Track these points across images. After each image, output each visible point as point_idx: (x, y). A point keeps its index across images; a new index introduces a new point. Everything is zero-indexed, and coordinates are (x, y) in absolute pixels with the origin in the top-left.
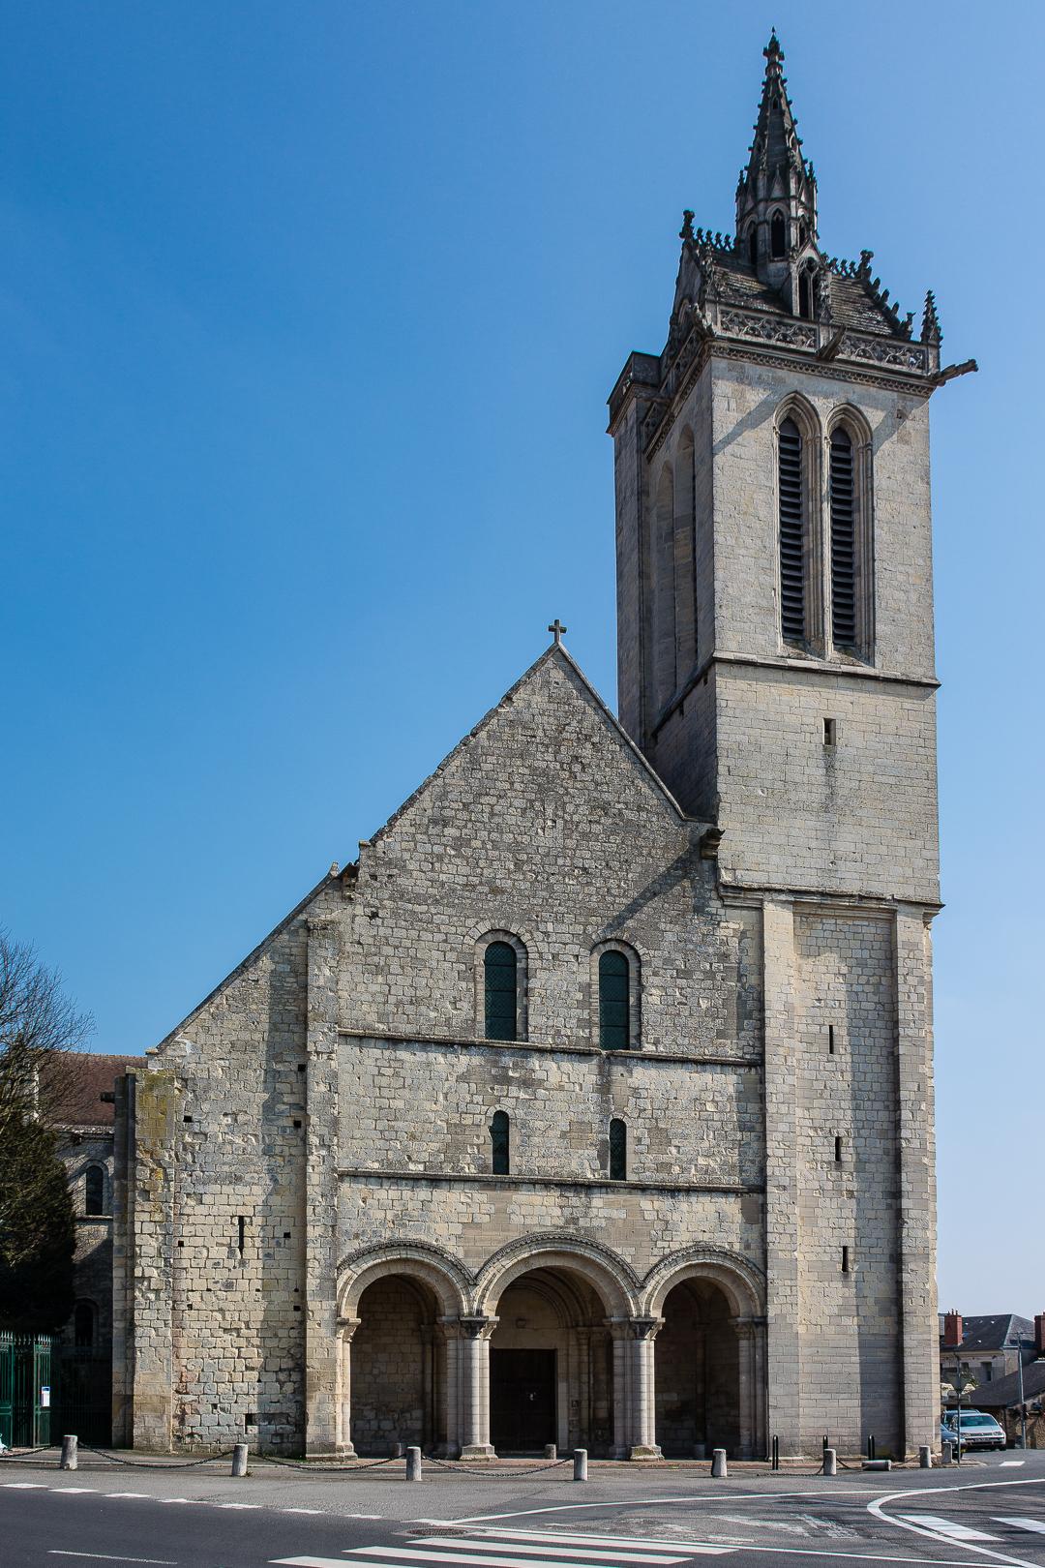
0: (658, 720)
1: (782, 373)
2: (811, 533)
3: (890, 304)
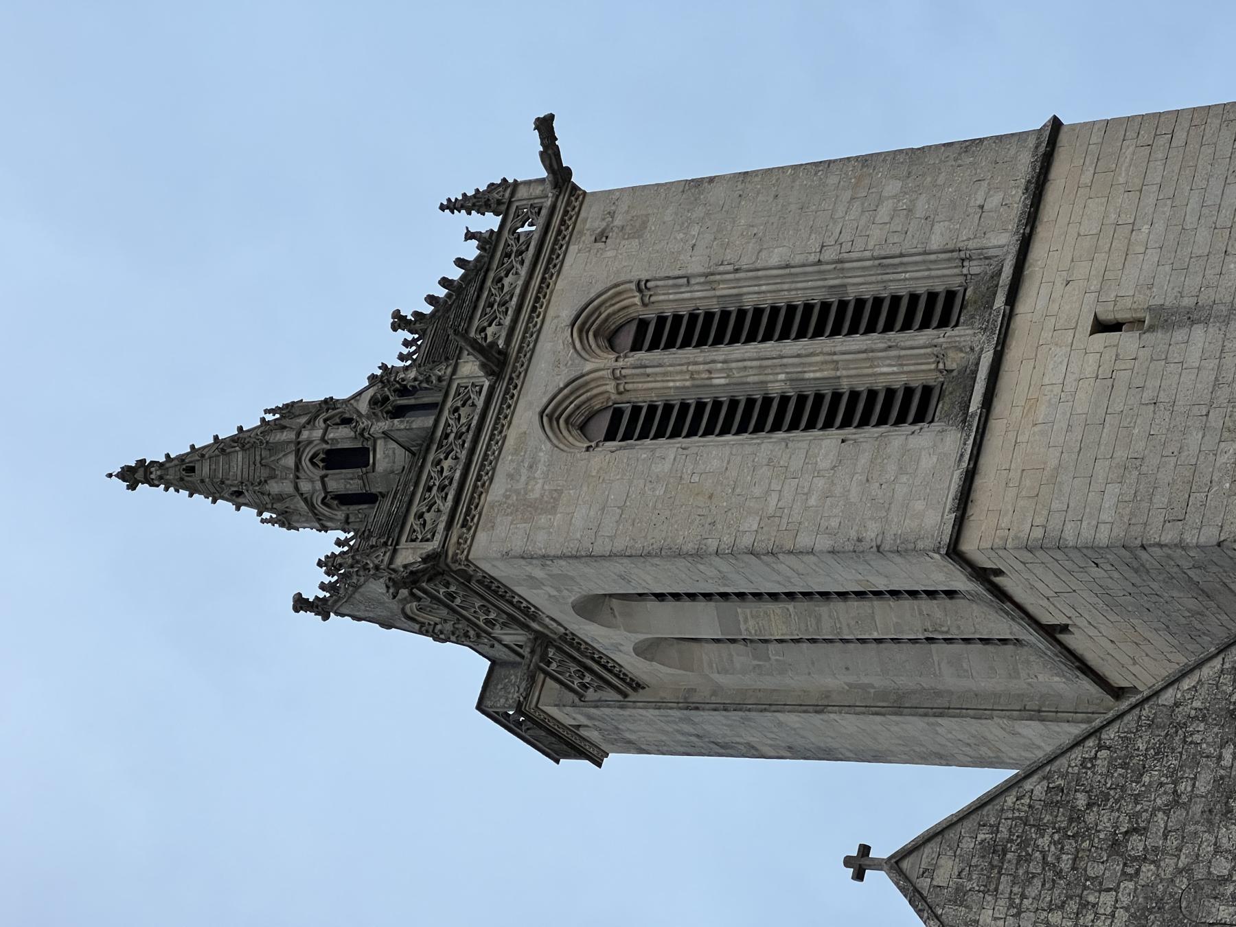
0: (1087, 686)
1: (512, 435)
2: (762, 378)
3: (456, 274)
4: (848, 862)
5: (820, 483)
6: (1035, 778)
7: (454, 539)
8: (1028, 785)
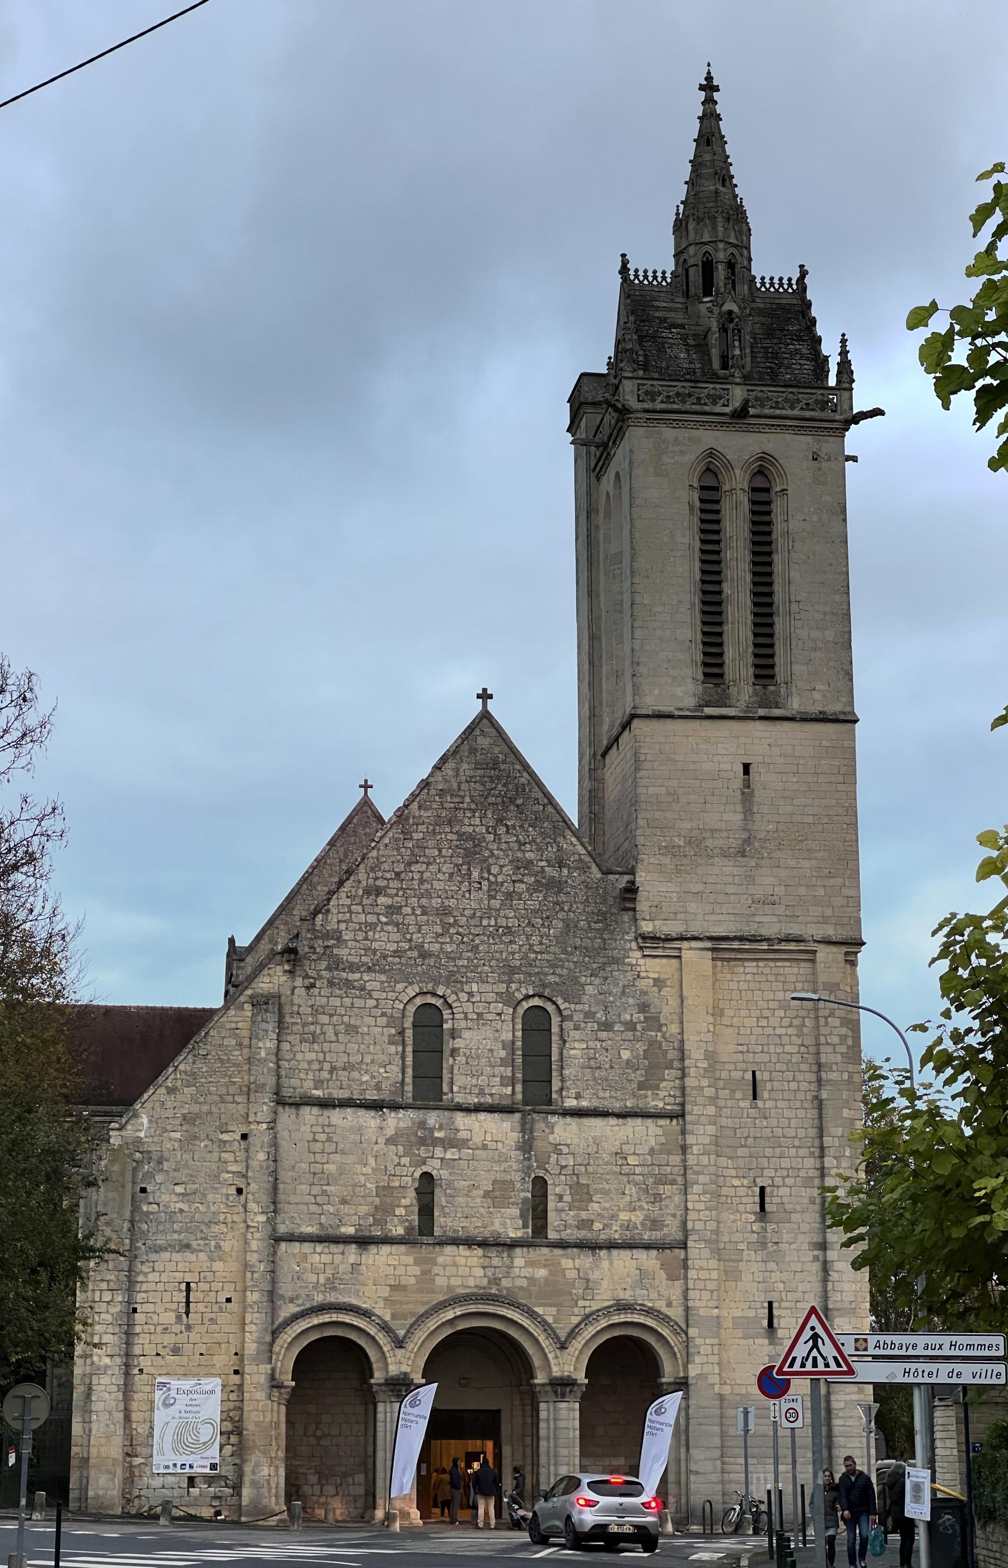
1: (700, 433)
4: (485, 690)
5: (668, 633)
6: (528, 777)
7: (639, 415)
8: (525, 774)
